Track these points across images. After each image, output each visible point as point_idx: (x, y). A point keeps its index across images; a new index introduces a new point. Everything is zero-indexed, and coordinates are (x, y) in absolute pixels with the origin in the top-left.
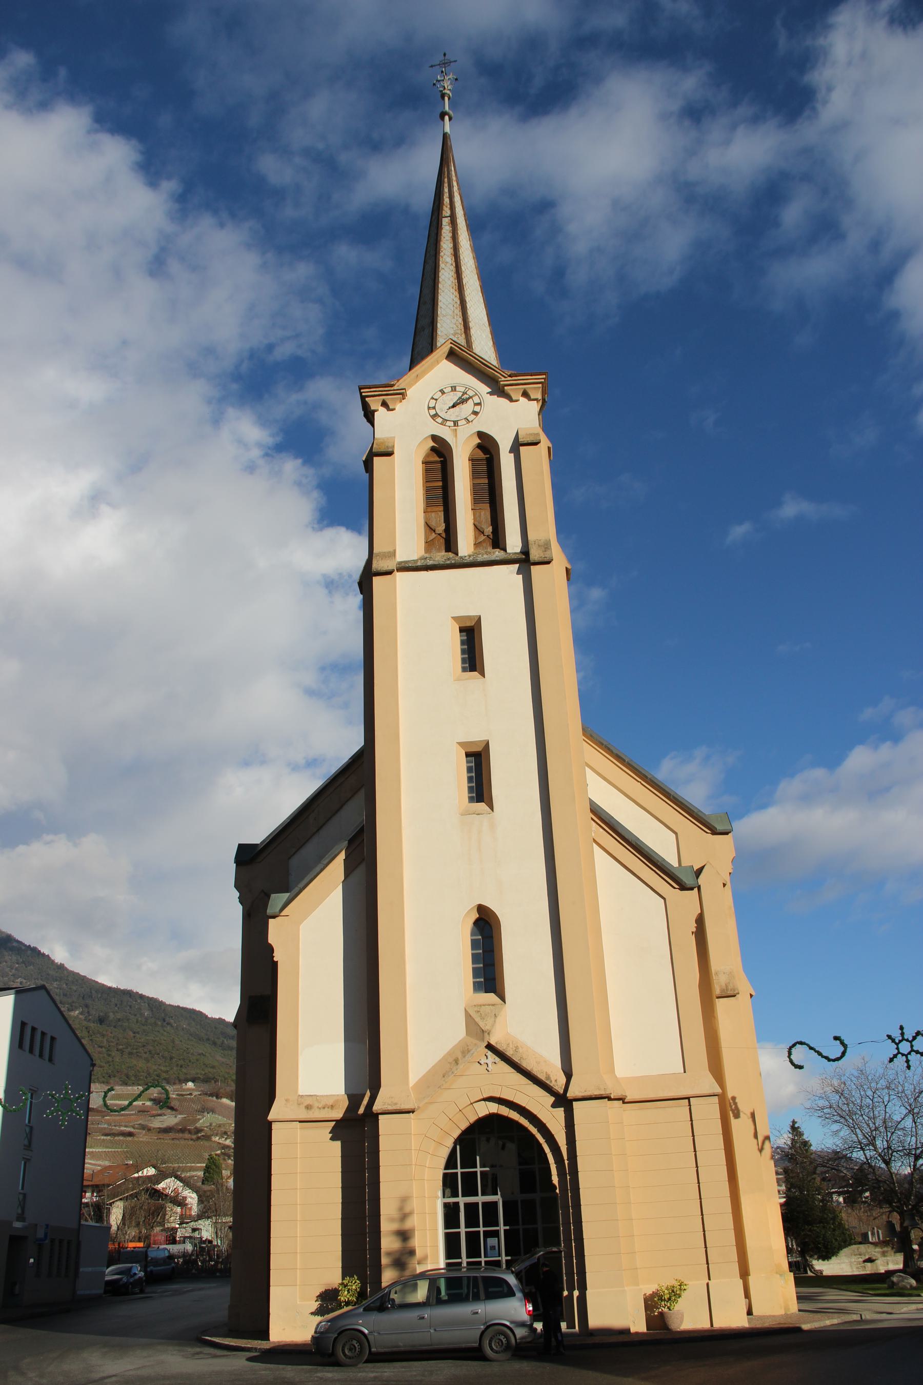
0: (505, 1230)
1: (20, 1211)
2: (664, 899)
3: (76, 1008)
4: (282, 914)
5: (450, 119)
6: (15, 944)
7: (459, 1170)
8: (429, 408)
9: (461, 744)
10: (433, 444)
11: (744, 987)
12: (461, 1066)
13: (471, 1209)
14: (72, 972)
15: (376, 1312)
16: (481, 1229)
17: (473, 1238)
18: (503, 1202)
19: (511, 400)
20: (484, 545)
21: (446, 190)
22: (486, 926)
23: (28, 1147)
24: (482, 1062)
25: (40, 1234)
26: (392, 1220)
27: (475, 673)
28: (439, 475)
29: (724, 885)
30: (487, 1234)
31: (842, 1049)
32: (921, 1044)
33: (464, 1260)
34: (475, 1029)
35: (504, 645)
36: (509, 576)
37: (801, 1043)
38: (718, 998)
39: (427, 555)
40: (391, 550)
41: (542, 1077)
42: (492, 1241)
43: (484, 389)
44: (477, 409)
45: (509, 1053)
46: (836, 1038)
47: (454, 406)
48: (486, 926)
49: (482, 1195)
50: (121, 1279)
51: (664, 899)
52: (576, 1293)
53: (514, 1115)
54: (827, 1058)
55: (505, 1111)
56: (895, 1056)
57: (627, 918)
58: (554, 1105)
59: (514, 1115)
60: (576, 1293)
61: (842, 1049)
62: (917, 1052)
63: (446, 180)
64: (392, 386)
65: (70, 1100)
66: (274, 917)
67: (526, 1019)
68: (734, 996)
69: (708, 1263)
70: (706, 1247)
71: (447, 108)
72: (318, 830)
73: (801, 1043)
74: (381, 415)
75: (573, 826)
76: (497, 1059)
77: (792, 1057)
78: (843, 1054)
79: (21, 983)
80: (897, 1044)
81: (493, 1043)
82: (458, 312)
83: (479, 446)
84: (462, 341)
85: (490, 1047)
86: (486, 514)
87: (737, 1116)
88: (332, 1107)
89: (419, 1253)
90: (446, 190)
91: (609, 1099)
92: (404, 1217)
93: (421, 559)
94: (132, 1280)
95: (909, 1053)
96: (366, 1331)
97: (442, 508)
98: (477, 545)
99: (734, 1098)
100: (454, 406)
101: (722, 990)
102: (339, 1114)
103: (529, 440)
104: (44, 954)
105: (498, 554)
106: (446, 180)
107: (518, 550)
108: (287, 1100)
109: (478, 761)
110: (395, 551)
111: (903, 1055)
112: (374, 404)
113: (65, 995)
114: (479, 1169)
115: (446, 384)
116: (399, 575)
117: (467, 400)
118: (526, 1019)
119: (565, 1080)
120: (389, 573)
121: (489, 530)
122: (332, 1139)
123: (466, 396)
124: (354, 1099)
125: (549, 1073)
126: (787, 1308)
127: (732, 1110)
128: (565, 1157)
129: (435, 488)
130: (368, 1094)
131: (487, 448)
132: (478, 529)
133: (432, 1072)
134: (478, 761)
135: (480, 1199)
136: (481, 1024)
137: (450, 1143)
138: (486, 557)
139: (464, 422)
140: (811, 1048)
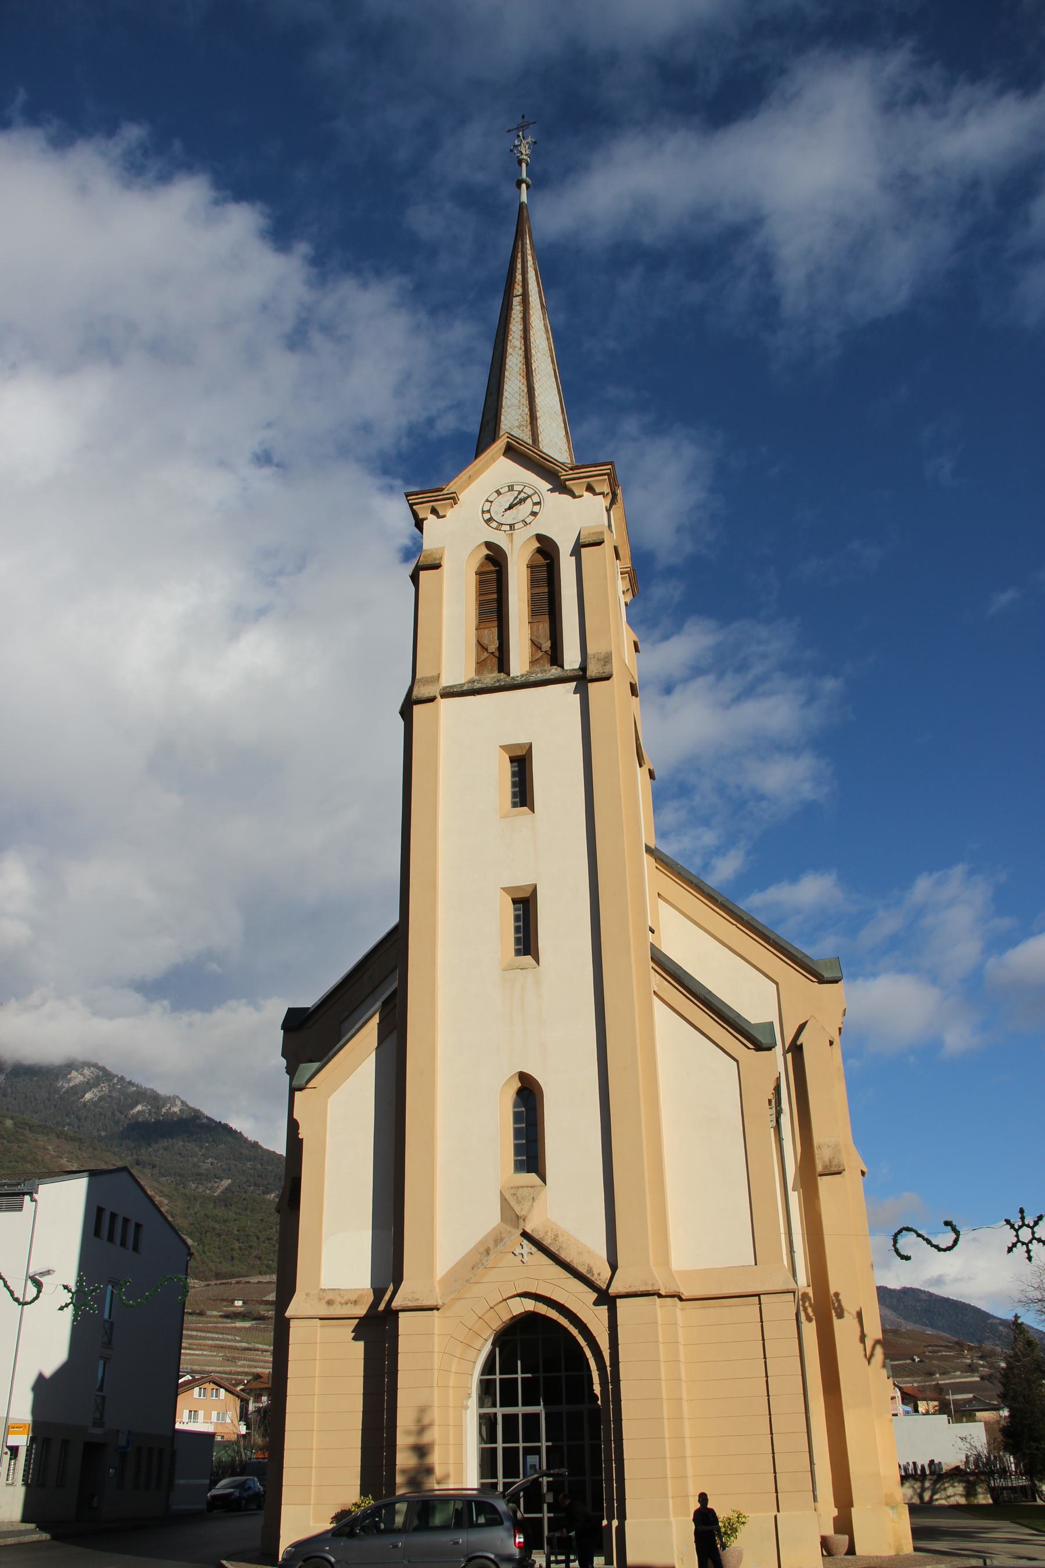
0: (547, 1447)
1: (98, 1415)
2: (737, 1061)
3: (272, 1191)
4: (309, 1085)
5: (528, 187)
6: (205, 1121)
7: (498, 1377)
8: (483, 512)
9: (506, 890)
10: (487, 552)
11: (853, 1161)
12: (492, 1257)
13: (510, 1420)
14: (268, 1151)
15: (345, 1538)
16: (521, 1445)
17: (510, 1455)
18: (546, 1414)
19: (574, 496)
20: (542, 662)
21: (519, 266)
22: (529, 1096)
23: (108, 1344)
24: (516, 1252)
25: (122, 1441)
26: (408, 1433)
27: (526, 808)
28: (494, 587)
29: (831, 1043)
30: (528, 1451)
31: (954, 1236)
32: (1044, 1231)
33: (501, 1480)
34: (510, 1215)
35: (557, 777)
36: (565, 695)
37: (908, 1229)
38: (820, 1175)
39: (477, 678)
40: (435, 674)
41: (583, 1270)
42: (532, 1459)
43: (544, 486)
44: (536, 509)
45: (547, 1242)
46: (947, 1223)
47: (511, 507)
48: (529, 1096)
49: (523, 1405)
50: (231, 1494)
51: (737, 1061)
52: (615, 1523)
53: (553, 1314)
54: (937, 1247)
55: (543, 1309)
56: (1014, 1245)
57: (692, 1084)
58: (596, 1303)
59: (553, 1314)
60: (615, 1523)
61: (954, 1236)
62: (1039, 1240)
63: (520, 255)
64: (442, 490)
65: (85, 1292)
66: (300, 1089)
67: (569, 1205)
68: (840, 1173)
69: (777, 1492)
70: (775, 1472)
71: (524, 175)
72: (372, 992)
73: (908, 1229)
74: (431, 523)
75: (632, 977)
76: (534, 1249)
77: (898, 1246)
78: (955, 1242)
79: (212, 1164)
80: (1017, 1231)
81: (528, 1230)
82: (525, 402)
83: (539, 551)
84: (526, 436)
85: (525, 1235)
86: (544, 627)
87: (840, 1316)
88: (355, 1302)
89: (438, 1471)
90: (519, 266)
91: (660, 1296)
92: (422, 1430)
93: (469, 682)
94: (245, 1495)
95: (1030, 1242)
96: (333, 1560)
97: (495, 624)
98: (533, 662)
99: (837, 1295)
100: (511, 507)
101: (825, 1167)
102: (362, 1311)
103: (591, 540)
104: (236, 1131)
105: (554, 672)
106: (520, 255)
107: (577, 666)
108: (307, 1295)
109: (525, 907)
110: (439, 675)
111: (1023, 1243)
112: (423, 512)
113: (260, 1176)
114: (520, 1376)
115: (502, 483)
116: (443, 703)
117: (524, 500)
118: (569, 1205)
119: (610, 1273)
120: (432, 700)
121: (547, 645)
122: (355, 1339)
123: (522, 495)
124: (378, 1293)
125: (592, 1264)
126: (899, 1548)
127: (835, 1309)
128: (608, 1363)
129: (489, 601)
130: (391, 1287)
131: (546, 551)
132: (535, 645)
133: (461, 1264)
134: (525, 907)
135: (520, 1410)
136: (517, 1209)
137: (488, 1347)
138: (540, 676)
139: (521, 525)
140: (919, 1235)
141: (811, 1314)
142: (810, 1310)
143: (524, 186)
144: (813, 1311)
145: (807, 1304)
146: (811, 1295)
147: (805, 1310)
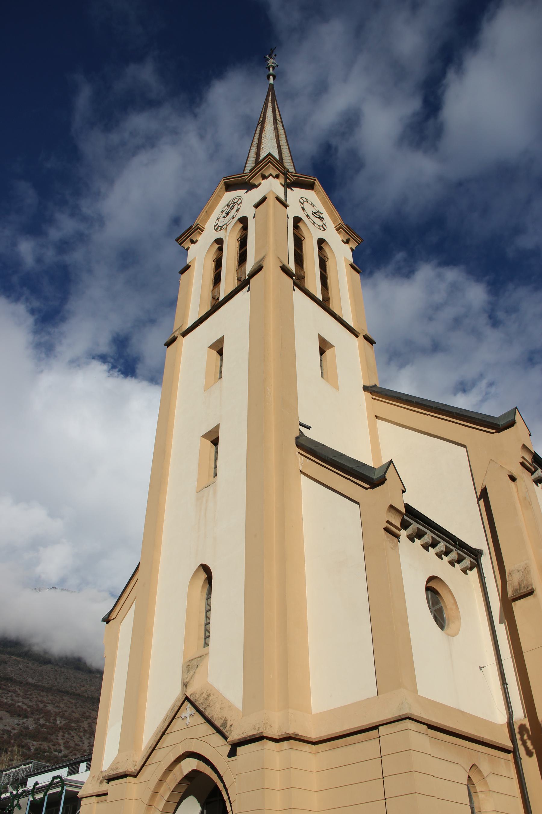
9: (204, 436)
101: (515, 591)
141: (531, 747)
142: (529, 743)
143: (271, 77)
144: (532, 744)
145: (525, 737)
146: (528, 726)
147: (524, 743)
